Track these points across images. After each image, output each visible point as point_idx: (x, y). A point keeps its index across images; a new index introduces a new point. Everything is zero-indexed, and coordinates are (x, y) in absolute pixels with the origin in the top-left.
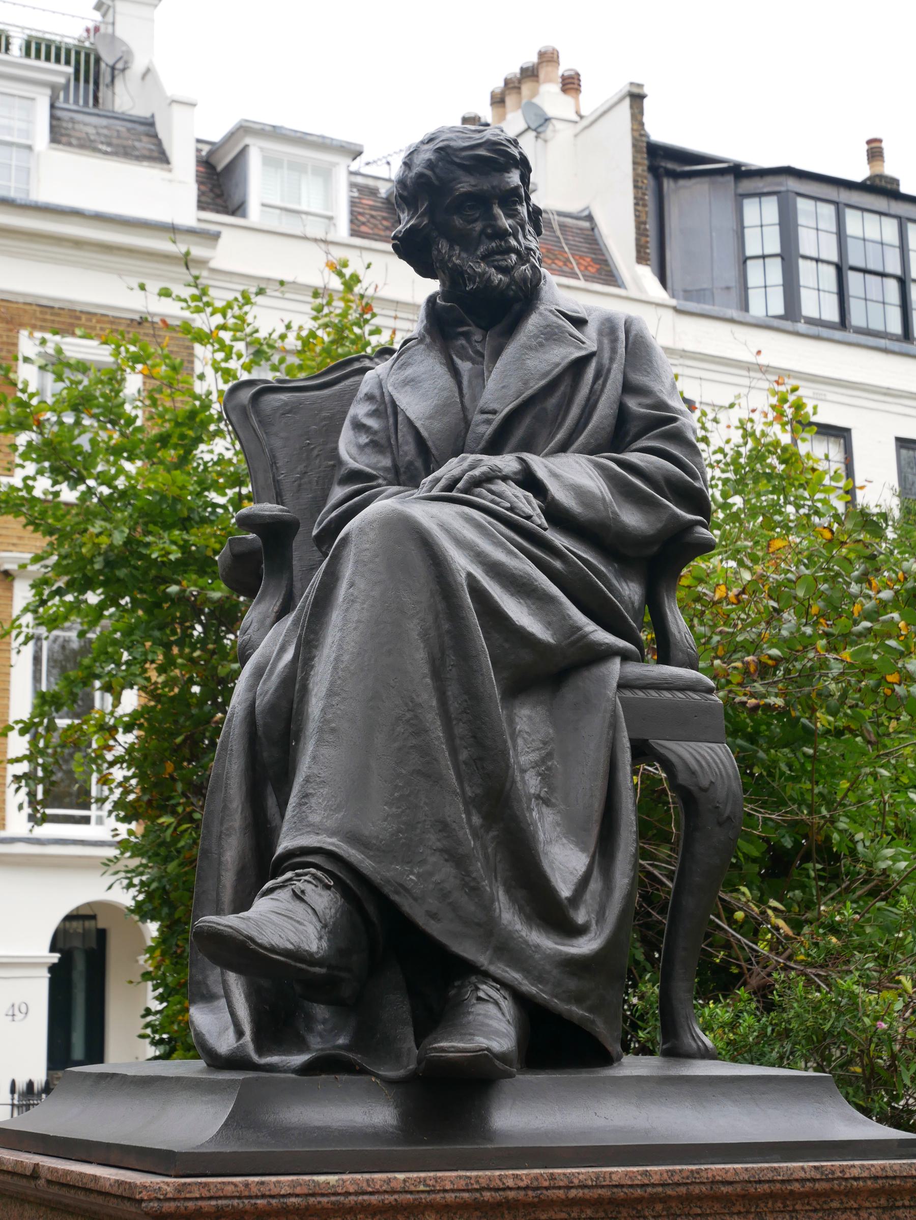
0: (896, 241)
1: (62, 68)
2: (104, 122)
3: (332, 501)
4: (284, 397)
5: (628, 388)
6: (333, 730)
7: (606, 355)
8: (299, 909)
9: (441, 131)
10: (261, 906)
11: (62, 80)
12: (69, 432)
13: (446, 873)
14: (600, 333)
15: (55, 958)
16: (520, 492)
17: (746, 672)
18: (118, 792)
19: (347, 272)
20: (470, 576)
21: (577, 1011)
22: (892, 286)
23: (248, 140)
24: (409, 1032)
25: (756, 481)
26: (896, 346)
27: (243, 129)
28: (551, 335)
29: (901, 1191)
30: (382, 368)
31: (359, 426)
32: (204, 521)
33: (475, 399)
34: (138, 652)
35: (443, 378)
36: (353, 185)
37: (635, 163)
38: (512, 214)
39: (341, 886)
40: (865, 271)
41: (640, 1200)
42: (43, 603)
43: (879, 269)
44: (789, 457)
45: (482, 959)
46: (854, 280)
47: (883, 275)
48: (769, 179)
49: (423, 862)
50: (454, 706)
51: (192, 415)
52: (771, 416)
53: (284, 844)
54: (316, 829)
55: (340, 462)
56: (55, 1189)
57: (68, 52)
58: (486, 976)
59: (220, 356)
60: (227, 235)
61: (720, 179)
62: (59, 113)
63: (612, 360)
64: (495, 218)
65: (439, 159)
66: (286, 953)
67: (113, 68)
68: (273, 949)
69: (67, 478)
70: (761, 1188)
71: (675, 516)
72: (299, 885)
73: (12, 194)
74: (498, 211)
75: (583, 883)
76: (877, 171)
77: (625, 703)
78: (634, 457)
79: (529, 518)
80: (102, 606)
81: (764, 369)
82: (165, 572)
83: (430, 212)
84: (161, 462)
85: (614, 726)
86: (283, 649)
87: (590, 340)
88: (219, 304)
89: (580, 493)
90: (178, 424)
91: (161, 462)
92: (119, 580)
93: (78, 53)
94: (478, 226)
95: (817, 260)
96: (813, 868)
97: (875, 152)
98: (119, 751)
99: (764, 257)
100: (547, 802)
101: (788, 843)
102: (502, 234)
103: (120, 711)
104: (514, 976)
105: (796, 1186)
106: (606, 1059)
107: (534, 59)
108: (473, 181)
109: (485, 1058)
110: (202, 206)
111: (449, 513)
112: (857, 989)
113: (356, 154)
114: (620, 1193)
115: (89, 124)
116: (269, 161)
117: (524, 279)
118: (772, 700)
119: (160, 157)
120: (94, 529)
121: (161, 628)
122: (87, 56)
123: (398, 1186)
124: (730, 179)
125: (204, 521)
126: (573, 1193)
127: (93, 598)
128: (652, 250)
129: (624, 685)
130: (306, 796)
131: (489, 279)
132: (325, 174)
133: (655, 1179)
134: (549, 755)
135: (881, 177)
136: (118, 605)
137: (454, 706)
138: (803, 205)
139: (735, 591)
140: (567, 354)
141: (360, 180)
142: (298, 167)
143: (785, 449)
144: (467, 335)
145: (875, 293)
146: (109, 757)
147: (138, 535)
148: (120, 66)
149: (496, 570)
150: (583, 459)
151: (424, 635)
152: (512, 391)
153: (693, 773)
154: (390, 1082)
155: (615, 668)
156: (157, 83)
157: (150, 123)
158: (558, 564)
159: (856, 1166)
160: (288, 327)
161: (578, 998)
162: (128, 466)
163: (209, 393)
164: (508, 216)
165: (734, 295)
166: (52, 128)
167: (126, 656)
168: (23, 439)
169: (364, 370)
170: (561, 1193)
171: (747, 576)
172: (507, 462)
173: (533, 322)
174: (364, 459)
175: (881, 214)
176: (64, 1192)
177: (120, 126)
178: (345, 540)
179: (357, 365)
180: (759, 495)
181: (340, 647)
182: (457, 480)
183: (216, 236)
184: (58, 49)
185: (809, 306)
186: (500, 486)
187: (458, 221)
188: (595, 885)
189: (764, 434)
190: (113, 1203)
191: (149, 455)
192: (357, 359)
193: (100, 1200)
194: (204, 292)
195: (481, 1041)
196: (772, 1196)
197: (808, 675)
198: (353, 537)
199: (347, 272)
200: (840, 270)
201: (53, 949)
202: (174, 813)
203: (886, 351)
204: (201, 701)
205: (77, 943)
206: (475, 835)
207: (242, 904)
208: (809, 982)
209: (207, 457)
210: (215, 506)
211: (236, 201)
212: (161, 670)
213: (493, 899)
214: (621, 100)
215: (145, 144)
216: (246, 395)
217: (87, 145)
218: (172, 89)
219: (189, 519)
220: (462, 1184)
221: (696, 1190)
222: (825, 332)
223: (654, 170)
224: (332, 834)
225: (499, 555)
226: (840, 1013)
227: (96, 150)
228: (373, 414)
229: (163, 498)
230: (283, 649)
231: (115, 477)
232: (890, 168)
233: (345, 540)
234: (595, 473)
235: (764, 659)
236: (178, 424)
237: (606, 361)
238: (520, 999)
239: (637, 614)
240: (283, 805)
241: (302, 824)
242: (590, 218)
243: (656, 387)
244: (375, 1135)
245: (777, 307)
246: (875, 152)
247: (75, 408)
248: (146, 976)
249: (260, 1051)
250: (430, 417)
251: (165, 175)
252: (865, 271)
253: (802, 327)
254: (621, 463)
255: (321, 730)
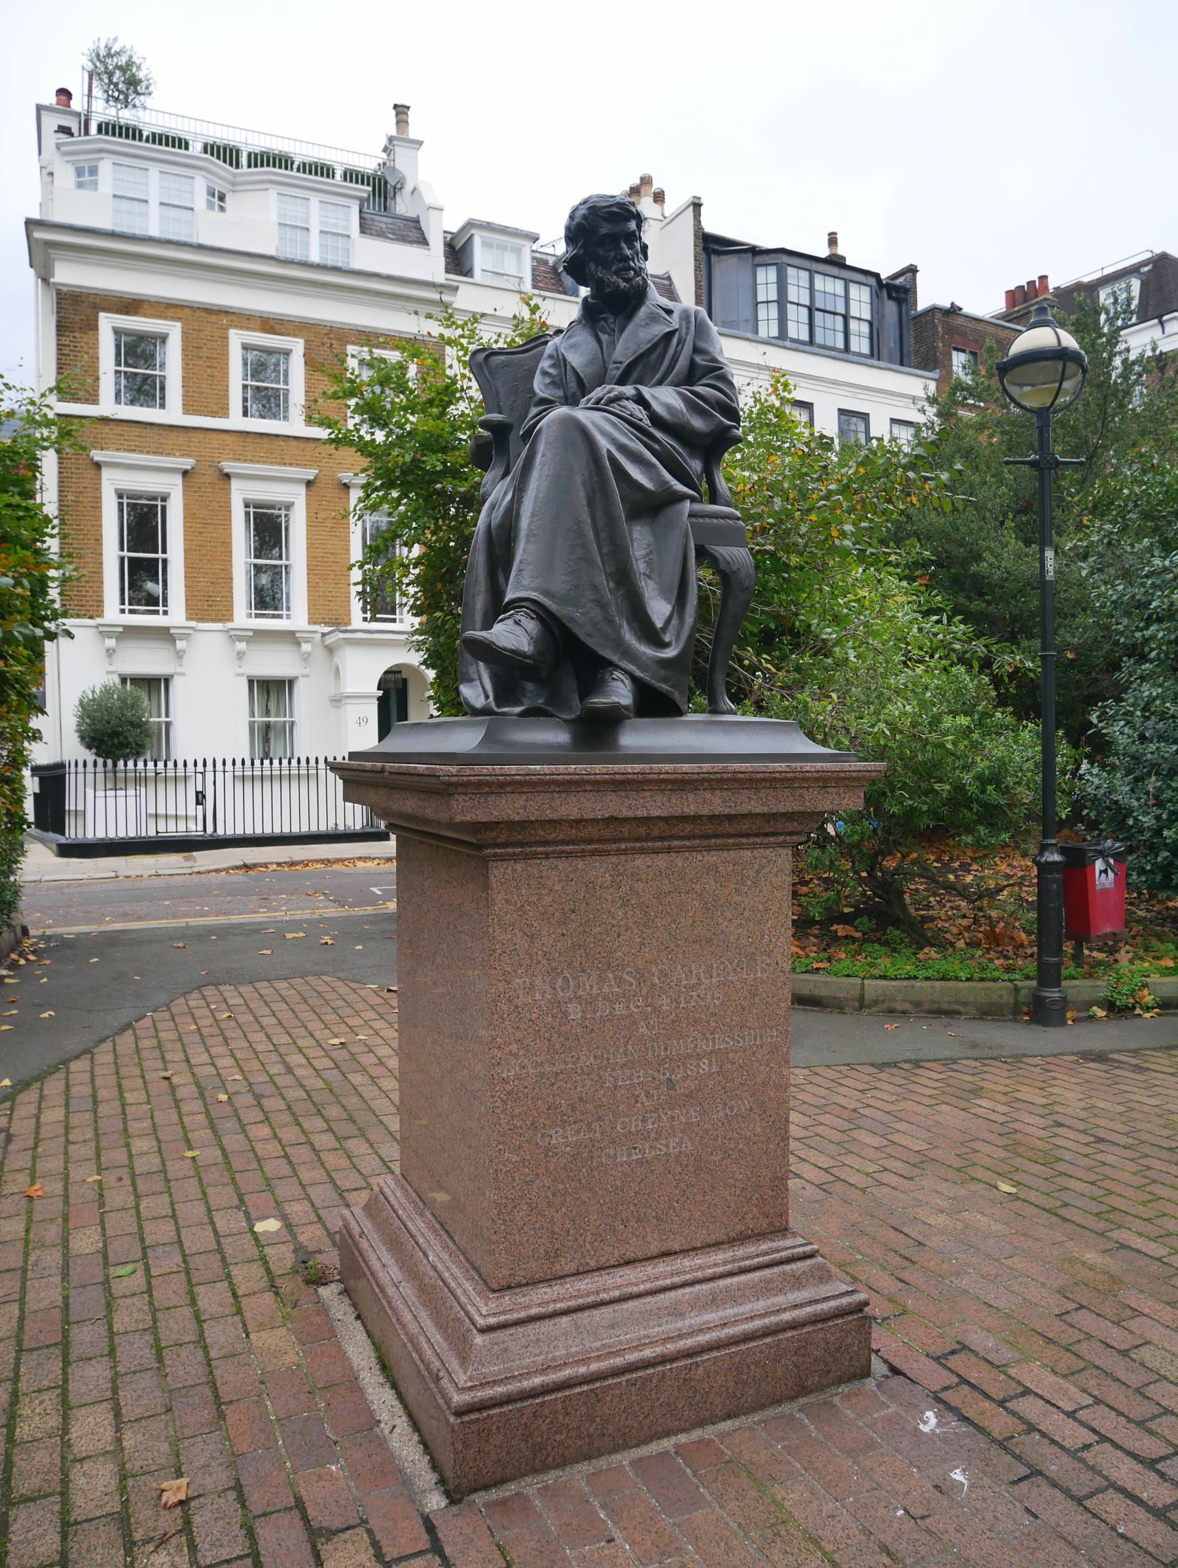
0: (843, 294)
1: (366, 188)
2: (390, 220)
3: (531, 415)
4: (502, 358)
5: (696, 350)
6: (534, 535)
7: (684, 331)
8: (518, 629)
9: (590, 197)
10: (498, 627)
11: (366, 195)
12: (378, 399)
13: (596, 613)
14: (681, 319)
15: (380, 693)
16: (636, 406)
17: (754, 531)
18: (412, 601)
19: (532, 303)
20: (608, 450)
21: (665, 687)
22: (840, 320)
23: (473, 231)
24: (577, 696)
25: (761, 428)
26: (840, 355)
27: (470, 225)
28: (653, 319)
29: (831, 779)
30: (557, 340)
31: (545, 373)
32: (455, 448)
33: (610, 355)
34: (421, 522)
35: (593, 344)
36: (533, 258)
37: (695, 245)
38: (631, 247)
39: (540, 619)
40: (825, 311)
41: (696, 780)
42: (368, 496)
43: (833, 310)
44: (779, 414)
45: (615, 659)
46: (818, 316)
47: (835, 314)
48: (772, 256)
49: (583, 607)
50: (600, 524)
51: (447, 387)
52: (771, 390)
53: (509, 596)
54: (526, 589)
55: (534, 393)
56: (394, 777)
57: (368, 178)
58: (617, 667)
59: (461, 353)
60: (462, 287)
61: (744, 255)
62: (365, 216)
63: (687, 334)
64: (622, 249)
65: (590, 214)
66: (512, 651)
67: (395, 188)
68: (505, 649)
69: (379, 424)
70: (759, 776)
71: (721, 422)
72: (517, 617)
73: (340, 265)
74: (624, 245)
75: (668, 621)
76: (834, 252)
77: (693, 525)
78: (698, 389)
79: (641, 420)
80: (399, 499)
81: (767, 368)
82: (434, 477)
83: (584, 246)
84: (430, 415)
85: (686, 537)
86: (505, 494)
87: (675, 322)
88: (460, 323)
89: (669, 408)
90: (439, 393)
91: (430, 415)
92: (409, 482)
93: (374, 179)
94: (612, 254)
95: (798, 304)
96: (786, 639)
97: (833, 240)
98: (411, 577)
99: (767, 302)
100: (649, 577)
101: (772, 626)
102: (626, 259)
103: (411, 556)
104: (632, 668)
105: (777, 775)
106: (680, 713)
107: (638, 182)
108: (609, 226)
109: (617, 707)
110: (448, 271)
111: (596, 416)
112: (809, 700)
113: (535, 239)
114: (686, 777)
115: (382, 222)
116: (485, 244)
117: (638, 285)
118: (768, 547)
119: (423, 241)
120: (395, 453)
121: (433, 509)
122: (380, 180)
123: (572, 771)
124: (750, 255)
125: (455, 448)
126: (662, 776)
127: (395, 494)
128: (704, 298)
129: (691, 515)
130: (521, 570)
131: (618, 286)
132: (518, 251)
133: (704, 770)
134: (651, 552)
135: (836, 255)
136: (408, 497)
137: (600, 524)
138: (791, 271)
139: (749, 486)
140: (659, 330)
141: (537, 255)
142: (502, 247)
143: (777, 410)
144: (605, 319)
145: (829, 325)
146: (406, 581)
147: (418, 456)
148: (398, 186)
149: (622, 448)
150: (670, 389)
151: (584, 483)
152: (631, 351)
153: (728, 563)
154: (565, 721)
155: (687, 504)
156: (421, 198)
157: (416, 221)
158: (656, 447)
159: (808, 766)
160: (499, 336)
161: (665, 681)
162: (411, 418)
163: (456, 375)
164: (629, 248)
165: (750, 325)
166: (361, 224)
167: (414, 525)
168: (352, 402)
169: (546, 343)
170: (656, 776)
171: (756, 478)
172: (629, 390)
173: (643, 311)
174: (548, 391)
175: (835, 277)
176: (399, 777)
177: (400, 223)
178: (539, 431)
179: (543, 340)
180: (762, 436)
181: (538, 490)
182: (601, 399)
183: (456, 289)
184: (363, 176)
185: (792, 332)
186: (625, 403)
187: (601, 251)
188: (674, 622)
189: (766, 401)
190: (425, 779)
191: (423, 411)
192: (543, 336)
193: (418, 779)
194: (451, 316)
195: (615, 699)
196: (764, 780)
197: (787, 532)
198: (544, 430)
199: (532, 303)
200: (811, 310)
201: (379, 689)
202: (442, 610)
203: (834, 358)
204: (455, 549)
205: (392, 686)
206: (611, 593)
207: (488, 626)
208: (783, 696)
209: (455, 412)
210: (461, 440)
211: (467, 268)
212: (433, 533)
213: (621, 627)
214: (688, 207)
215: (414, 234)
216: (482, 356)
217: (381, 235)
218: (429, 200)
219: (446, 447)
220: (605, 771)
221: (725, 776)
222: (801, 347)
223: (705, 249)
224: (535, 590)
225: (624, 440)
226: (798, 713)
227: (386, 237)
228: (553, 366)
229: (432, 435)
230: (505, 494)
231: (405, 424)
232: (841, 250)
233: (539, 431)
234: (677, 397)
235: (765, 525)
236: (439, 393)
237: (684, 334)
238: (634, 679)
239: (700, 478)
240: (507, 579)
241: (516, 588)
242: (669, 278)
243: (711, 350)
244: (560, 747)
245: (775, 332)
246: (833, 240)
247: (381, 384)
248: (430, 698)
249: (498, 706)
250: (586, 366)
251: (426, 252)
252: (825, 311)
253: (788, 344)
254: (692, 392)
255: (528, 536)
